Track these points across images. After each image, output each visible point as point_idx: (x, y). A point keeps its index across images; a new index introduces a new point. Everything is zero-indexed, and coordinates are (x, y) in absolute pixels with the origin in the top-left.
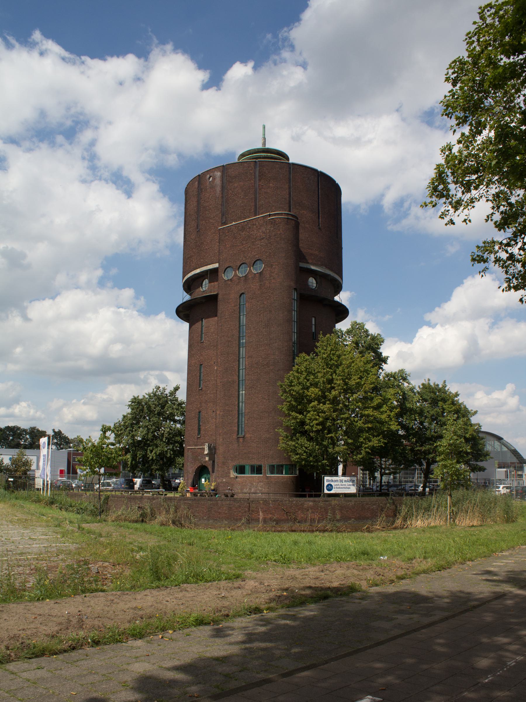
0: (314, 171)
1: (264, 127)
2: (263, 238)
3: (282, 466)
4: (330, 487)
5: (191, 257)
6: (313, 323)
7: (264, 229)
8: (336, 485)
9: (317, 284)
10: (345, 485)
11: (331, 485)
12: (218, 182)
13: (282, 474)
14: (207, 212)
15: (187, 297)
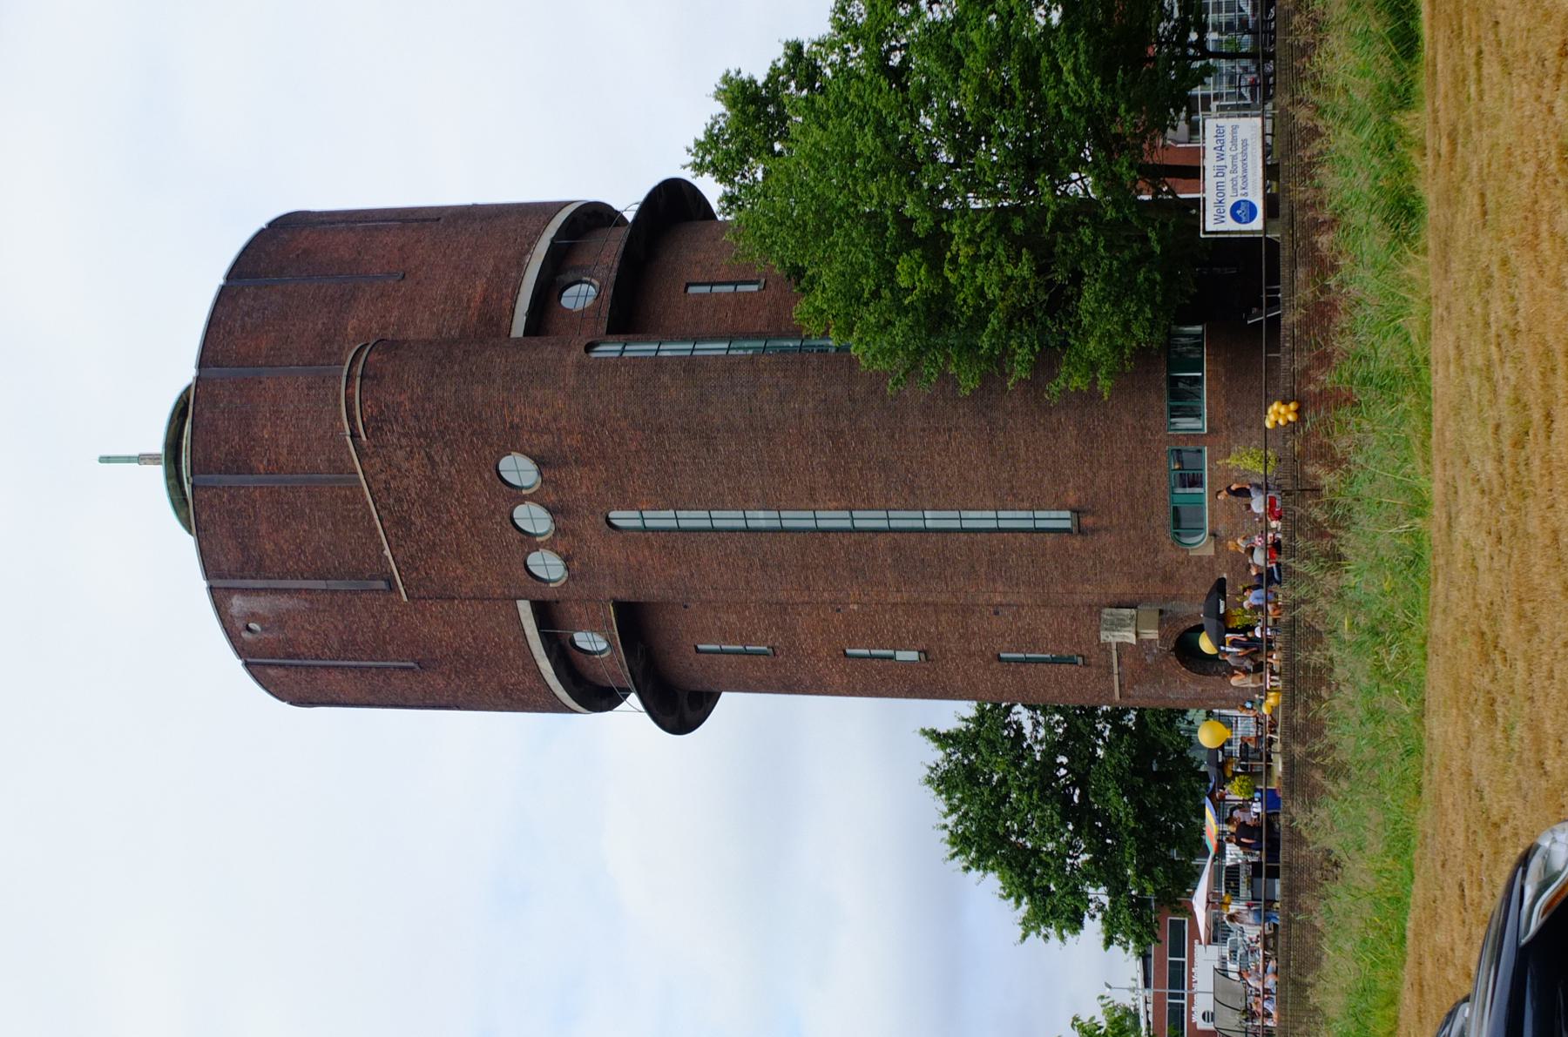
0: (224, 297)
1: (105, 459)
2: (430, 458)
3: (1173, 381)
4: (1242, 210)
5: (503, 688)
6: (706, 289)
7: (400, 453)
8: (1234, 187)
9: (581, 282)
10: (1234, 158)
11: (1236, 206)
12: (261, 604)
13: (1198, 380)
14: (359, 638)
15: (633, 699)
